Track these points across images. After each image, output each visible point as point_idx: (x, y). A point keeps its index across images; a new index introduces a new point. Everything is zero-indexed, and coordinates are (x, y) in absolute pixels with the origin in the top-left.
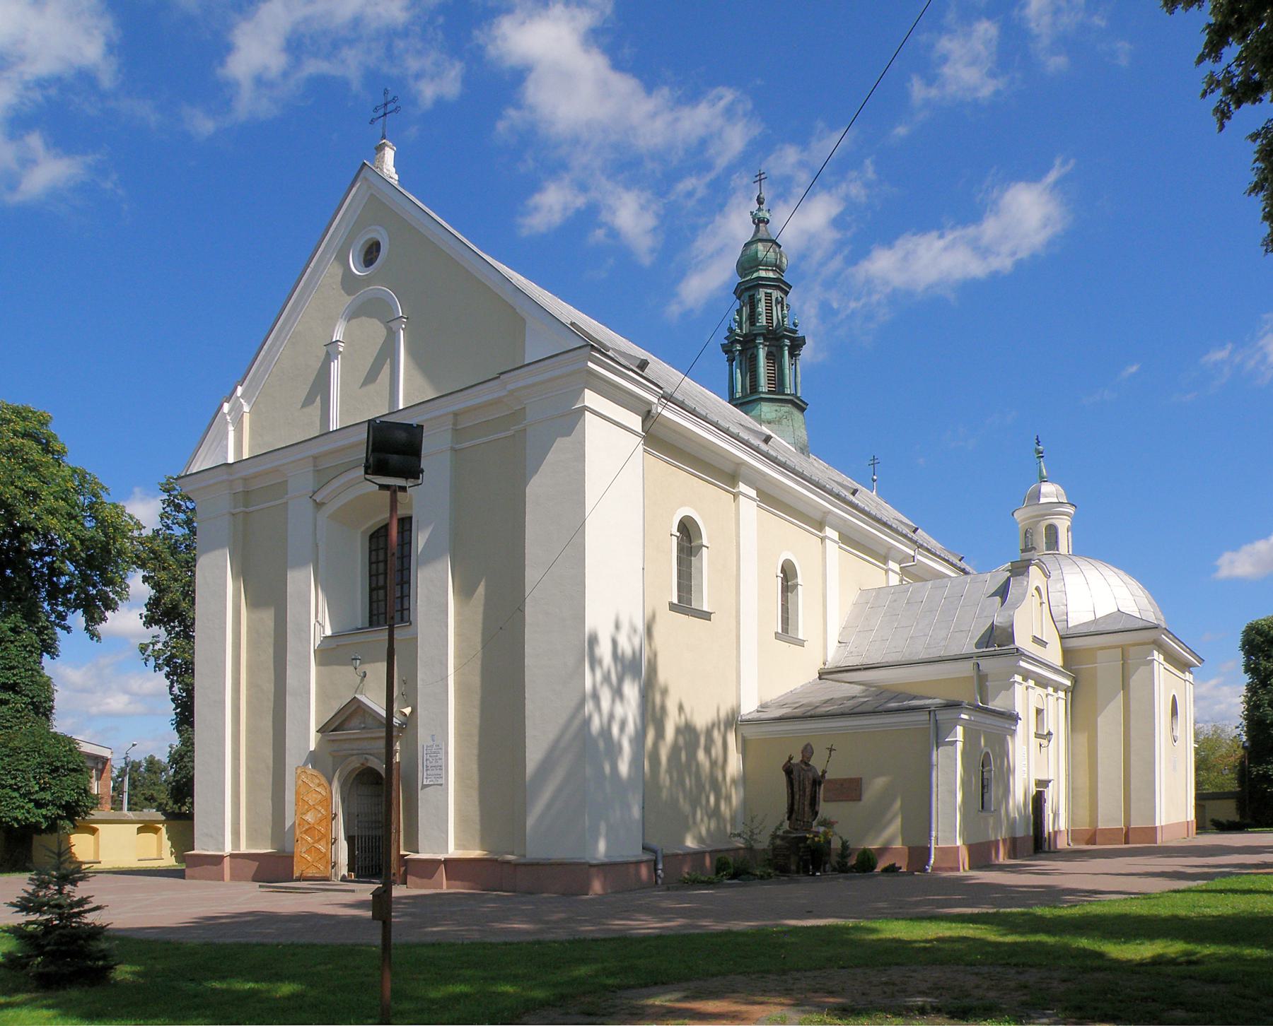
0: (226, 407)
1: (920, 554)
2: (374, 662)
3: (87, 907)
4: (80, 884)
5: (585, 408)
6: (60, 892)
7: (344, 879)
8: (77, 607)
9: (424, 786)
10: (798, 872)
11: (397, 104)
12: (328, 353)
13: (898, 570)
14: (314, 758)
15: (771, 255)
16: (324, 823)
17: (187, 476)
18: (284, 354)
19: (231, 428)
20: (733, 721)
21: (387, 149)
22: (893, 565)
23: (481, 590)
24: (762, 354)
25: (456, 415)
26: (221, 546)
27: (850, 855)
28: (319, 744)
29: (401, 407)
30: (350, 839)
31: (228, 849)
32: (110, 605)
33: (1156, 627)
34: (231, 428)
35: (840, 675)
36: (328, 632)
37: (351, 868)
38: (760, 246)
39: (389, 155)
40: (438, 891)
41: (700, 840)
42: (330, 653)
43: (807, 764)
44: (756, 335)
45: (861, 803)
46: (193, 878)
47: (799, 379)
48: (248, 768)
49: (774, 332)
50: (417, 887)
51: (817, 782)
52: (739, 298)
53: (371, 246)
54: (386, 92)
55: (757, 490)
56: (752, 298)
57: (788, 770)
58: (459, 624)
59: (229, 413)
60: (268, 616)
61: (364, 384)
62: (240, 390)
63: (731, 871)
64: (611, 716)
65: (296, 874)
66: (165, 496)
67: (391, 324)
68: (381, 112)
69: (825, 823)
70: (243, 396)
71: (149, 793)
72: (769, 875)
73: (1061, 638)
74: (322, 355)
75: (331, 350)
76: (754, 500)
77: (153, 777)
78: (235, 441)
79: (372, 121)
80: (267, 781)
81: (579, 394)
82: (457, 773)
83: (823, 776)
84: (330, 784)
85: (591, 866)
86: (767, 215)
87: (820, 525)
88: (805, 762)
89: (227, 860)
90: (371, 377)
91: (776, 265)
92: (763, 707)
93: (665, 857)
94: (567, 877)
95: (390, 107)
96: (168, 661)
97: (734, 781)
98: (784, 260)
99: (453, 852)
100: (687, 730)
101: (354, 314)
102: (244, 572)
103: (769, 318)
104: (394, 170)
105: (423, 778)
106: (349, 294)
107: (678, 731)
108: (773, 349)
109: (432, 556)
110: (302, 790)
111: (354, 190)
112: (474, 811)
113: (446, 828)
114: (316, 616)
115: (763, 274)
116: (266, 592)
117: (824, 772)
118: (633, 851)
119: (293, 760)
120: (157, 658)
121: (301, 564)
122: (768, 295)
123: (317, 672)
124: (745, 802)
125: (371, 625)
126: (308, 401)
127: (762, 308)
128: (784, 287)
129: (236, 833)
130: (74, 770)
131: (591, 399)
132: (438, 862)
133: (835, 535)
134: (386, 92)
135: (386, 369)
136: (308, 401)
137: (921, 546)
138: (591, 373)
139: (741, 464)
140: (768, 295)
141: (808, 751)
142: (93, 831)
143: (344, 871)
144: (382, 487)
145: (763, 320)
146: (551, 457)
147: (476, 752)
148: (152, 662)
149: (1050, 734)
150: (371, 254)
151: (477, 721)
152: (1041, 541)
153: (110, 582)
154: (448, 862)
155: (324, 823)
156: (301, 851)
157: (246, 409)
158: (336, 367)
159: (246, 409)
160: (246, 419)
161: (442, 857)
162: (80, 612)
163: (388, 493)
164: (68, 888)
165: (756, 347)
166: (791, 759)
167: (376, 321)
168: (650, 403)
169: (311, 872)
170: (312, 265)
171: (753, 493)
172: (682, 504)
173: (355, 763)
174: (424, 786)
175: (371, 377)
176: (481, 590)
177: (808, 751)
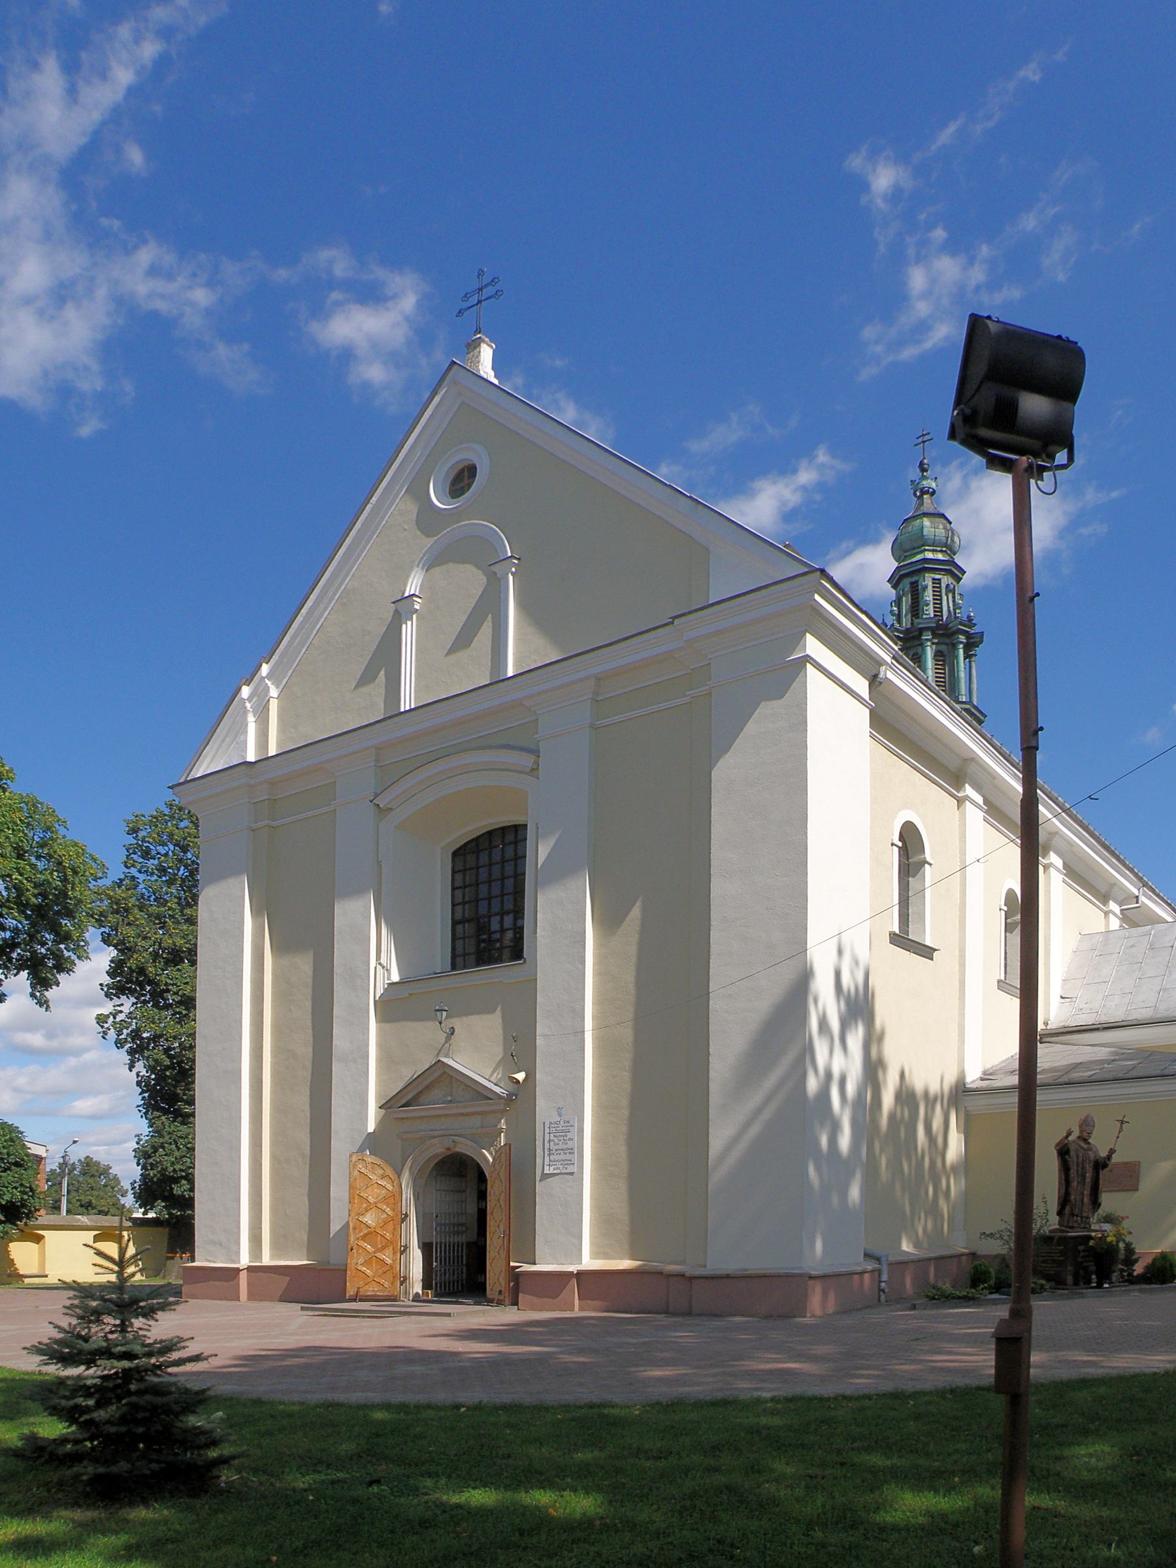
0: (245, 691)
1: (1145, 895)
2: (467, 1014)
3: (175, 1355)
4: (160, 1315)
5: (807, 659)
6: (123, 1328)
7: (416, 1298)
8: (19, 969)
9: (545, 1176)
10: (1076, 1283)
11: (498, 287)
12: (397, 612)
13: (1118, 912)
14: (373, 1143)
15: (941, 532)
16: (390, 1226)
17: (186, 782)
18: (328, 617)
19: (251, 719)
20: (960, 1093)
21: (483, 346)
22: (1113, 906)
23: (636, 912)
24: (929, 652)
25: (598, 679)
26: (234, 872)
27: (1136, 1261)
28: (381, 1124)
29: (510, 673)
30: (426, 1248)
31: (245, 1260)
32: (63, 966)
34: (251, 719)
35: (1068, 1037)
36: (395, 977)
37: (427, 1284)
38: (926, 522)
39: (486, 353)
40: (568, 1314)
41: (917, 1245)
42: (394, 1006)
43: (1085, 1141)
44: (921, 631)
45: (1137, 1194)
46: (194, 1297)
47: (975, 686)
48: (274, 1157)
49: (945, 627)
50: (533, 1308)
51: (1100, 1165)
52: (895, 587)
53: (462, 471)
54: (481, 273)
55: (986, 801)
56: (915, 585)
58: (600, 960)
59: (250, 699)
60: (304, 964)
61: (451, 651)
62: (265, 669)
63: (992, 1282)
64: (829, 1075)
65: (351, 1291)
66: (130, 840)
67: (495, 568)
68: (474, 300)
69: (1108, 1219)
70: (270, 676)
71: (85, 1199)
72: (1042, 1287)
74: (388, 616)
75: (402, 607)
77: (91, 1181)
78: (259, 729)
79: (460, 313)
80: (301, 1172)
81: (797, 640)
82: (596, 1158)
83: (1109, 1157)
84: (399, 1177)
85: (811, 1277)
86: (934, 485)
89: (243, 1276)
90: (463, 640)
91: (946, 545)
92: (987, 1075)
94: (769, 1297)
96: (135, 1035)
97: (954, 1168)
98: (956, 539)
99: (588, 1262)
100: (906, 1096)
101: (433, 563)
102: (267, 905)
103: (938, 610)
104: (492, 373)
105: (544, 1164)
106: (428, 536)
107: (898, 1096)
108: (943, 648)
109: (560, 871)
110: (359, 1183)
111: (437, 399)
112: (621, 1210)
113: (578, 1231)
114: (377, 958)
115: (929, 555)
116: (302, 930)
117: (1112, 1151)
118: (855, 1262)
119: (342, 1147)
120: (119, 1033)
121: (355, 891)
122: (937, 582)
123: (381, 1034)
124: (967, 1196)
125: (454, 967)
126: (366, 679)
127: (929, 596)
129: (256, 1240)
130: (17, 1164)
131: (813, 646)
132: (570, 1274)
134: (481, 273)
135: (486, 629)
136: (366, 679)
137: (1145, 885)
138: (817, 610)
139: (973, 759)
140: (937, 582)
141: (1087, 1125)
142: (38, 1239)
143: (418, 1288)
146: (751, 728)
147: (624, 1129)
148: (112, 1034)
150: (462, 480)
151: (627, 1087)
153: (65, 937)
154: (580, 1275)
155: (390, 1226)
156: (357, 1261)
157: (274, 692)
158: (409, 631)
159: (274, 692)
160: (274, 706)
161: (573, 1268)
162: (24, 974)
164: (138, 1322)
165: (921, 645)
166: (1069, 1134)
167: (470, 568)
168: (880, 662)
169: (371, 1290)
170: (374, 499)
171: (979, 799)
173: (438, 1148)
174: (545, 1176)
175: (463, 640)
176: (636, 912)
177: (1087, 1125)
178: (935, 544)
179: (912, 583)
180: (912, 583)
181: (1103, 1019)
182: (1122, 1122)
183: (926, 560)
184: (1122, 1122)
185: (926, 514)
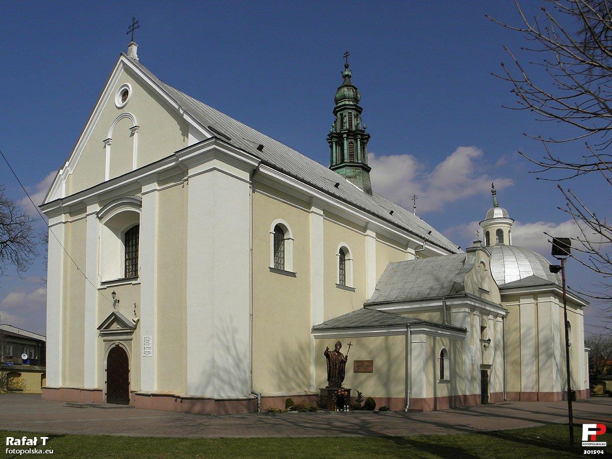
33: (553, 284)
38: (345, 89)
43: (338, 352)
54: (134, 19)
55: (324, 211)
57: (327, 354)
68: (131, 29)
73: (500, 289)
76: (322, 216)
86: (350, 73)
87: (364, 229)
88: (337, 351)
93: (262, 397)
95: (136, 26)
103: (351, 125)
115: (347, 103)
127: (346, 119)
128: (359, 110)
133: (374, 235)
139: (312, 197)
144: (558, 259)
145: (347, 126)
149: (489, 340)
152: (494, 238)
163: (560, 260)
171: (321, 212)
172: (282, 218)
178: (349, 99)
179: (341, 114)
180: (341, 114)
181: (388, 299)
182: (350, 345)
183: (345, 105)
184: (350, 345)
185: (346, 86)
